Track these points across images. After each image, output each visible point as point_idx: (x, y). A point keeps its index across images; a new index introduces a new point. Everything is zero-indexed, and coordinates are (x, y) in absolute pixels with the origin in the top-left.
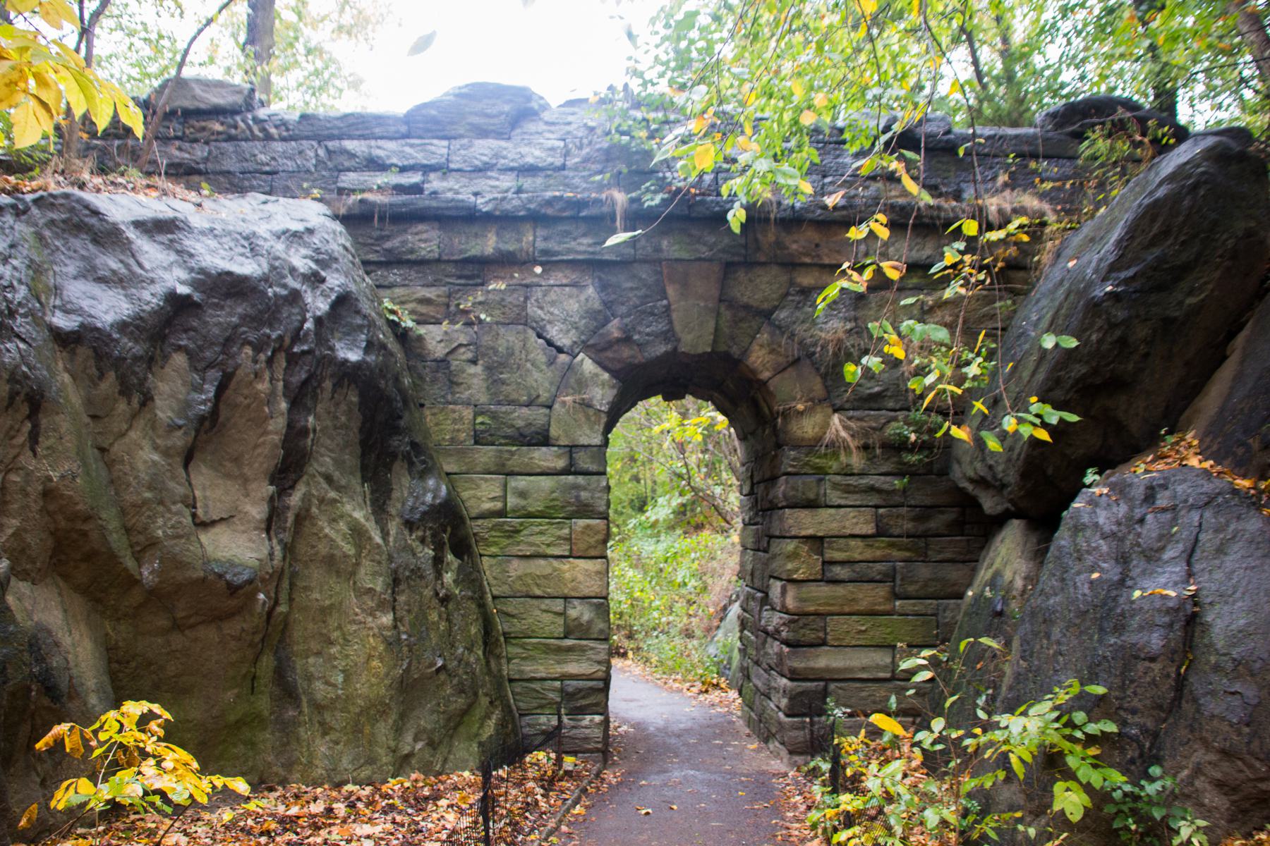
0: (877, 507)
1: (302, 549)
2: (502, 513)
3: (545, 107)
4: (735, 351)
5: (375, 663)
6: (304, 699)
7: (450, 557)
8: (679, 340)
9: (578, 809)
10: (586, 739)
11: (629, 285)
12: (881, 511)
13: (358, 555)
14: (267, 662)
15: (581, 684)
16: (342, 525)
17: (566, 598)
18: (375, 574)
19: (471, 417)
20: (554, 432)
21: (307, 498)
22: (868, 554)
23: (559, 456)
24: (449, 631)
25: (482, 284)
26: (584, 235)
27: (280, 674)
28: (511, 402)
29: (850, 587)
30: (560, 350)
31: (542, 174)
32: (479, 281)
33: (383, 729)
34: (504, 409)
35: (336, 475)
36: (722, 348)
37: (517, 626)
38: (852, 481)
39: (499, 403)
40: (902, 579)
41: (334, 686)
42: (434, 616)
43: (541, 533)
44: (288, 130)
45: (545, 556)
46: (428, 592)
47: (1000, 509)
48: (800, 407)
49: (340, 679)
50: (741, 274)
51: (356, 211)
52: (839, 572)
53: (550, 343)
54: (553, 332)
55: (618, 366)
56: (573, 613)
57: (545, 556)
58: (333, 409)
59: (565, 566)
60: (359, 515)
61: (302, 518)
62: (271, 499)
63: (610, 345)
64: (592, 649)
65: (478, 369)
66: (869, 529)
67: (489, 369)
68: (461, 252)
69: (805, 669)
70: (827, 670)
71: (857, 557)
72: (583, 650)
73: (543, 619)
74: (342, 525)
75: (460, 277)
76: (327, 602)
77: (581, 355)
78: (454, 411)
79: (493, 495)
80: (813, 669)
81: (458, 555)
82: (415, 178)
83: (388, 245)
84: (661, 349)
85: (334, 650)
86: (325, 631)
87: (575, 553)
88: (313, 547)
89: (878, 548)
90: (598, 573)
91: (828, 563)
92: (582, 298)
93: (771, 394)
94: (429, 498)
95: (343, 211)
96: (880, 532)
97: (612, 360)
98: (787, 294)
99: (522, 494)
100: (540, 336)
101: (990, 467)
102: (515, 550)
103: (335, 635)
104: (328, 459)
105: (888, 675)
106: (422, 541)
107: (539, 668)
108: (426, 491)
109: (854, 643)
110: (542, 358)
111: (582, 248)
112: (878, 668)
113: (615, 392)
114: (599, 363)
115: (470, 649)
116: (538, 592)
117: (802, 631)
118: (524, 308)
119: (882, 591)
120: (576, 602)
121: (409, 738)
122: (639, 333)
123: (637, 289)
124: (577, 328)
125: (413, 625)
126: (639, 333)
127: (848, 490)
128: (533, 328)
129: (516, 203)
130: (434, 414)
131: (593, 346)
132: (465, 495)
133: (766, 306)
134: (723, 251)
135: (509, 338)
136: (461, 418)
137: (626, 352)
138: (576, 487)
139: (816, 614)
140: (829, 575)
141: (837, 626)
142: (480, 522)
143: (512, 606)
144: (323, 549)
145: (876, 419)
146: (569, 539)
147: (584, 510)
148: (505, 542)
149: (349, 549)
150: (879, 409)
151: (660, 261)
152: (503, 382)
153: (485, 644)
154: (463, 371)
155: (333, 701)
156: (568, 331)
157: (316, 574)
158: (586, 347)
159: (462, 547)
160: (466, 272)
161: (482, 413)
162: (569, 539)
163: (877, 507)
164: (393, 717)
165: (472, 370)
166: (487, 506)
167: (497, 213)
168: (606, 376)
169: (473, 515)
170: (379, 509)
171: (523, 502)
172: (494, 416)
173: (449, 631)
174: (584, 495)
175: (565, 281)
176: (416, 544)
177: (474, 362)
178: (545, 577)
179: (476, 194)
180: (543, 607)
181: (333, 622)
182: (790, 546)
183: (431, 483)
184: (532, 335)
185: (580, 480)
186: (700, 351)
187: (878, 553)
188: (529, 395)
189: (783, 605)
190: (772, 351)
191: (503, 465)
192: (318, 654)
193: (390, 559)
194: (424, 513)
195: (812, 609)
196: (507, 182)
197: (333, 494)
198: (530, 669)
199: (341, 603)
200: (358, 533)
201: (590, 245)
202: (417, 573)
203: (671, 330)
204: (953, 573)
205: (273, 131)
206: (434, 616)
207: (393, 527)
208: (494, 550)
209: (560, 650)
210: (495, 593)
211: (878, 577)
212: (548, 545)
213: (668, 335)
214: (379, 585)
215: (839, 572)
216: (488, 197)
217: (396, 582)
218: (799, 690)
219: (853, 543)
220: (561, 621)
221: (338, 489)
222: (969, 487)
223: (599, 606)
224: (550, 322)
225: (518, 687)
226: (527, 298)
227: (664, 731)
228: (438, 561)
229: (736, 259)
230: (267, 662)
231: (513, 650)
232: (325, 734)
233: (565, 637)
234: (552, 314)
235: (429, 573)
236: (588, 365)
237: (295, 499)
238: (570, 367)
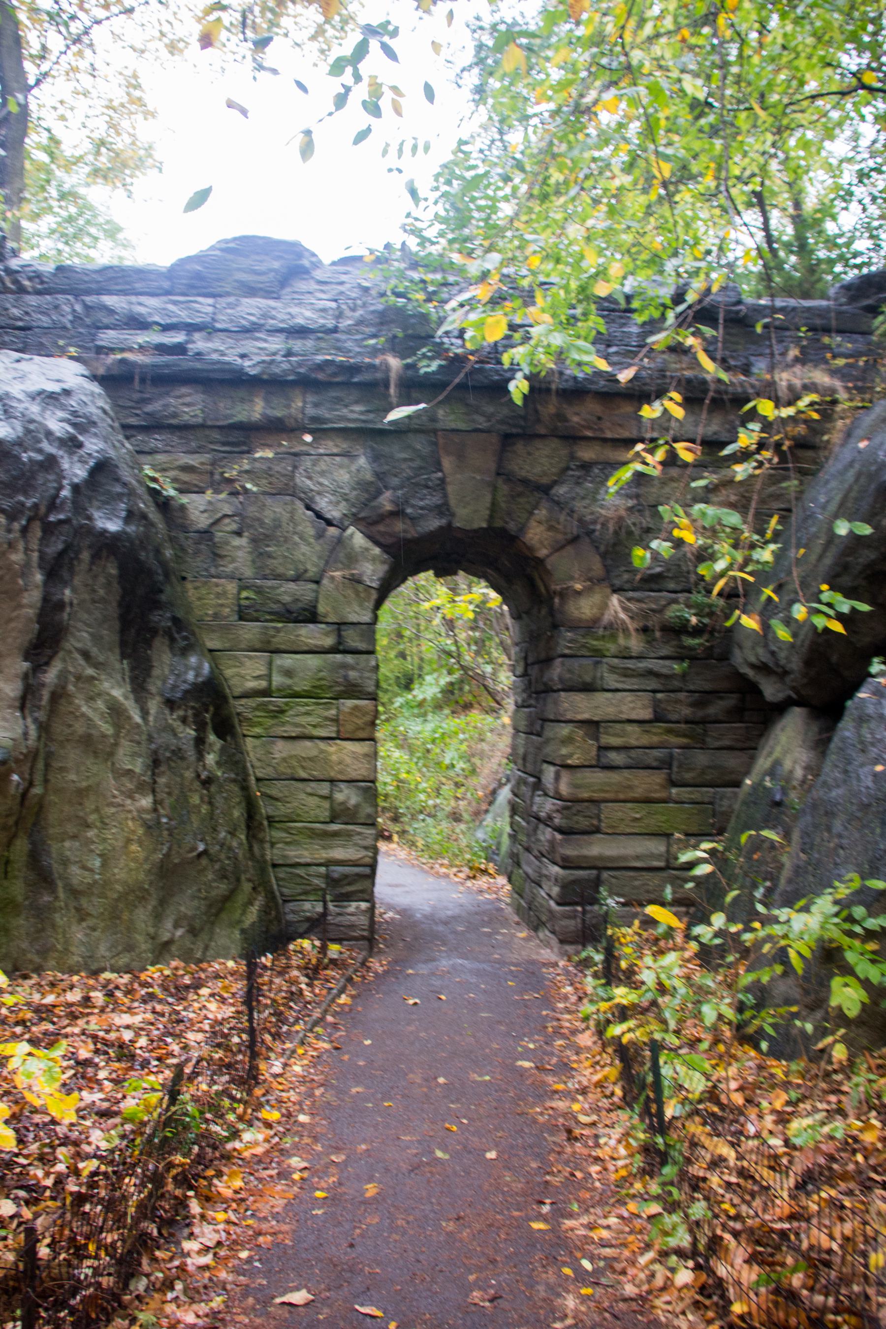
0: (654, 691)
1: (58, 728)
3: (317, 265)
4: (512, 526)
5: (134, 847)
6: (60, 884)
7: (212, 738)
8: (453, 515)
9: (343, 999)
10: (352, 927)
11: (403, 455)
12: (659, 696)
13: (117, 735)
14: (21, 846)
16: (100, 704)
17: (332, 781)
18: (134, 755)
19: (235, 591)
20: (321, 609)
21: (63, 675)
22: (645, 740)
23: (327, 634)
24: (211, 815)
25: (248, 452)
26: (357, 402)
27: (35, 858)
28: (278, 577)
29: (626, 773)
30: (329, 523)
31: (312, 336)
32: (245, 448)
33: (142, 916)
34: (270, 583)
35: (94, 651)
36: (498, 524)
37: (281, 810)
38: (630, 664)
39: (265, 577)
40: (680, 766)
41: (91, 870)
42: (195, 799)
43: (307, 714)
44: (42, 282)
45: (311, 738)
46: (189, 774)
47: (781, 696)
49: (97, 863)
50: (520, 447)
51: (115, 371)
52: (615, 758)
53: (319, 515)
54: (323, 504)
55: (389, 541)
56: (339, 797)
57: (311, 738)
58: (90, 582)
59: (332, 748)
61: (58, 696)
62: (25, 676)
63: (382, 518)
64: (359, 834)
65: (242, 542)
66: (646, 714)
67: (254, 541)
68: (227, 417)
69: (578, 857)
70: (601, 858)
71: (634, 742)
72: (349, 835)
74: (100, 704)
75: (224, 444)
76: (84, 784)
77: (352, 529)
78: (217, 585)
79: (258, 673)
80: (585, 857)
81: (220, 735)
82: (179, 338)
83: (149, 408)
84: (434, 523)
85: (91, 834)
86: (81, 814)
87: (343, 735)
88: (70, 726)
89: (655, 734)
90: (366, 755)
92: (354, 468)
93: (548, 572)
94: (191, 676)
95: (101, 371)
96: (658, 718)
97: (383, 534)
98: (568, 468)
99: (288, 673)
100: (308, 508)
101: (773, 653)
102: (280, 731)
103: (93, 818)
104: (85, 635)
105: (662, 864)
106: (184, 720)
107: (304, 853)
108: (188, 668)
109: (628, 830)
110: (311, 531)
111: (355, 416)
112: (652, 856)
113: (385, 567)
114: (369, 537)
116: (303, 774)
117: (575, 818)
118: (292, 478)
119: (657, 778)
120: (342, 786)
121: (169, 924)
122: (413, 506)
123: (411, 460)
124: (346, 500)
125: (173, 808)
126: (413, 506)
127: (626, 673)
128: (301, 499)
129: (285, 366)
130: (196, 588)
131: (363, 519)
132: (228, 673)
133: (545, 481)
134: (502, 422)
136: (225, 593)
137: (399, 526)
138: (345, 666)
139: (591, 801)
140: (604, 761)
141: (612, 813)
142: (243, 701)
144: (80, 728)
145: (656, 600)
146: (336, 720)
147: (352, 690)
148: (270, 722)
149: (107, 728)
150: (660, 591)
151: (435, 431)
152: (270, 556)
153: (249, 827)
154: (227, 543)
155: (90, 886)
156: (338, 503)
157: (72, 755)
158: (356, 520)
160: (231, 439)
161: (246, 588)
162: (336, 720)
163: (654, 691)
164: (153, 902)
165: (237, 542)
166: (252, 684)
167: (265, 377)
168: (377, 551)
169: (236, 694)
171: (289, 681)
172: (259, 591)
173: (211, 815)
174: (353, 674)
175: (335, 451)
176: (177, 725)
177: (239, 534)
179: (243, 356)
180: (309, 790)
181: (90, 805)
182: (565, 730)
183: (193, 660)
184: (300, 506)
185: (349, 659)
186: (476, 526)
187: (655, 739)
188: (296, 569)
189: (557, 791)
190: (551, 528)
191: (269, 642)
192: (74, 837)
193: (150, 739)
195: (585, 795)
196: (276, 344)
197: (90, 671)
199: (98, 784)
200: (116, 712)
201: (362, 413)
202: (178, 753)
203: (446, 504)
204: (731, 761)
205: (26, 283)
206: (195, 799)
207: (154, 706)
208: (258, 730)
209: (326, 835)
210: (260, 775)
211: (655, 764)
212: (314, 726)
213: (443, 509)
214: (138, 766)
215: (615, 758)
216: (257, 359)
217: (155, 763)
218: (572, 878)
219: (629, 728)
220: (326, 804)
221: (97, 665)
222: (750, 673)
223: (366, 790)
224: (319, 493)
225: (282, 873)
226: (295, 467)
227: (431, 918)
228: (200, 742)
229: (514, 431)
230: (21, 846)
231: (277, 834)
232: (82, 920)
234: (321, 484)
235: (191, 754)
236: (358, 539)
237: (51, 676)
238: (340, 541)
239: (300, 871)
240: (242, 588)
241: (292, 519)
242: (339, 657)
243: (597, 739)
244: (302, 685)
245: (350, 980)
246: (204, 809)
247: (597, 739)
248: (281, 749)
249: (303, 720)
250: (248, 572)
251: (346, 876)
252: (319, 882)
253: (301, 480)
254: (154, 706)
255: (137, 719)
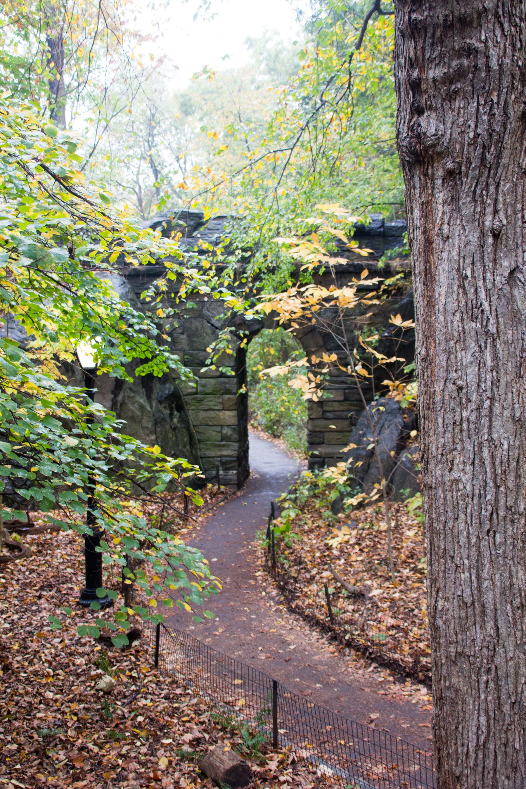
2: (196, 393)
7: (176, 413)
9: (222, 503)
10: (231, 480)
13: (142, 415)
15: (228, 459)
16: (136, 405)
17: (222, 426)
18: (148, 421)
21: (124, 398)
22: (341, 408)
24: (176, 441)
28: (198, 350)
34: (195, 352)
37: (203, 437)
42: (170, 435)
45: (213, 410)
46: (168, 427)
48: (313, 350)
51: (132, 273)
52: (329, 415)
53: (212, 325)
56: (224, 432)
57: (213, 410)
59: (221, 414)
60: (141, 401)
61: (123, 404)
62: (112, 400)
65: (184, 337)
66: (341, 398)
67: (189, 336)
71: (336, 409)
72: (228, 446)
73: (213, 434)
74: (136, 405)
81: (179, 411)
91: (325, 412)
94: (167, 392)
95: (127, 273)
96: (346, 399)
106: (165, 408)
107: (213, 453)
108: (166, 389)
110: (210, 332)
115: (184, 447)
118: (202, 311)
125: (163, 439)
135: (196, 324)
138: (224, 383)
139: (320, 432)
143: (201, 429)
146: (222, 403)
149: (139, 413)
152: (195, 342)
153: (190, 444)
159: (180, 408)
161: (187, 354)
162: (222, 403)
170: (149, 397)
172: (191, 355)
173: (176, 441)
174: (227, 386)
176: (163, 409)
177: (183, 333)
178: (213, 418)
183: (167, 385)
184: (205, 321)
185: (226, 380)
187: (345, 408)
193: (154, 415)
194: (166, 398)
195: (318, 430)
197: (132, 395)
198: (208, 453)
200: (142, 407)
202: (164, 420)
206: (170, 435)
207: (154, 404)
208: (193, 407)
209: (219, 446)
214: (150, 425)
215: (329, 415)
217: (156, 424)
219: (334, 404)
220: (219, 435)
221: (134, 392)
225: (204, 460)
227: (273, 478)
228: (171, 415)
231: (202, 446)
233: (222, 441)
235: (168, 419)
237: (120, 398)
239: (210, 459)
240: (184, 355)
241: (202, 327)
242: (222, 379)
243: (322, 408)
244: (209, 390)
245: (226, 498)
246: (174, 439)
247: (322, 408)
248: (202, 414)
249: (210, 403)
250: (187, 348)
251: (227, 461)
252: (218, 463)
253: (205, 312)
254: (154, 404)
255: (149, 409)
